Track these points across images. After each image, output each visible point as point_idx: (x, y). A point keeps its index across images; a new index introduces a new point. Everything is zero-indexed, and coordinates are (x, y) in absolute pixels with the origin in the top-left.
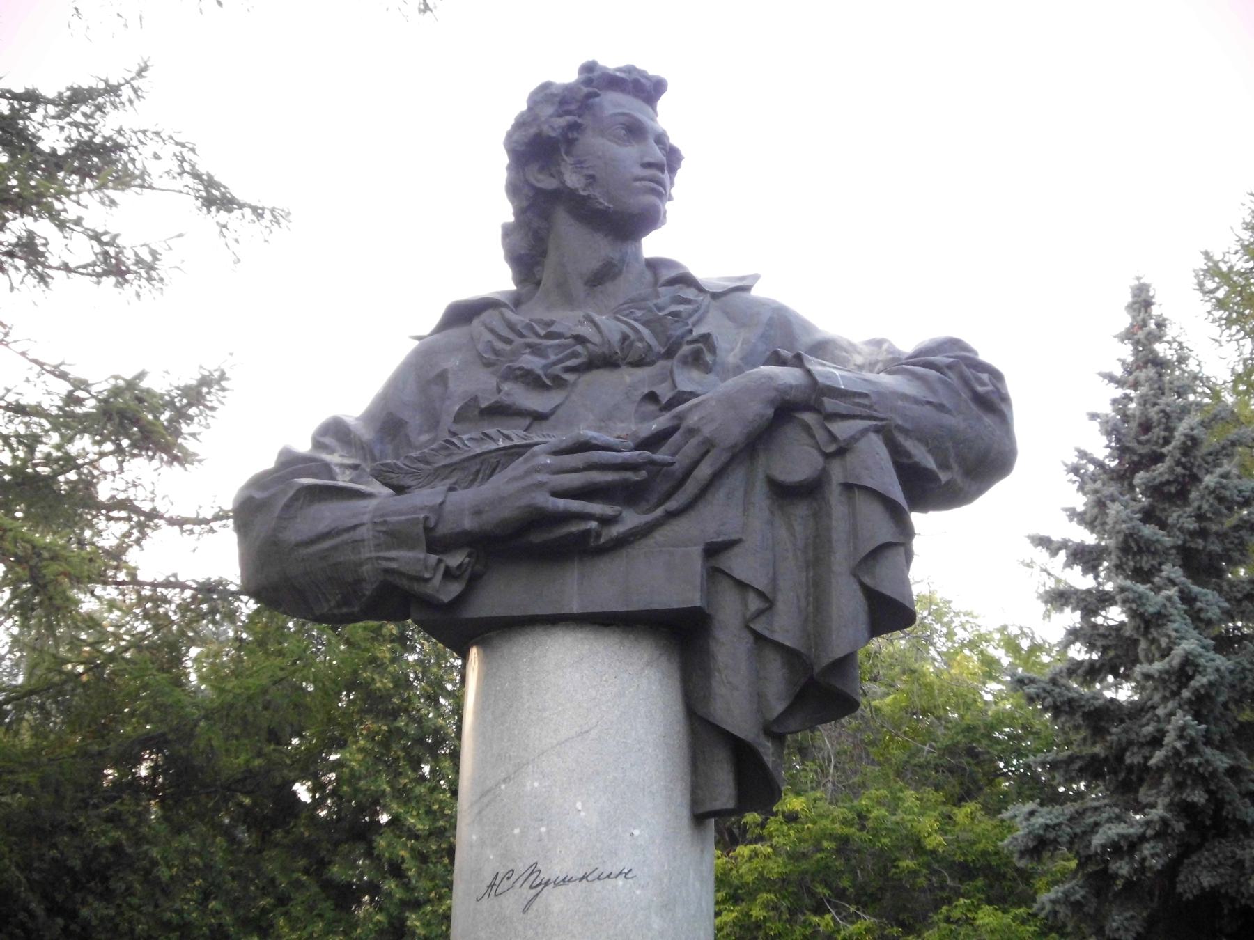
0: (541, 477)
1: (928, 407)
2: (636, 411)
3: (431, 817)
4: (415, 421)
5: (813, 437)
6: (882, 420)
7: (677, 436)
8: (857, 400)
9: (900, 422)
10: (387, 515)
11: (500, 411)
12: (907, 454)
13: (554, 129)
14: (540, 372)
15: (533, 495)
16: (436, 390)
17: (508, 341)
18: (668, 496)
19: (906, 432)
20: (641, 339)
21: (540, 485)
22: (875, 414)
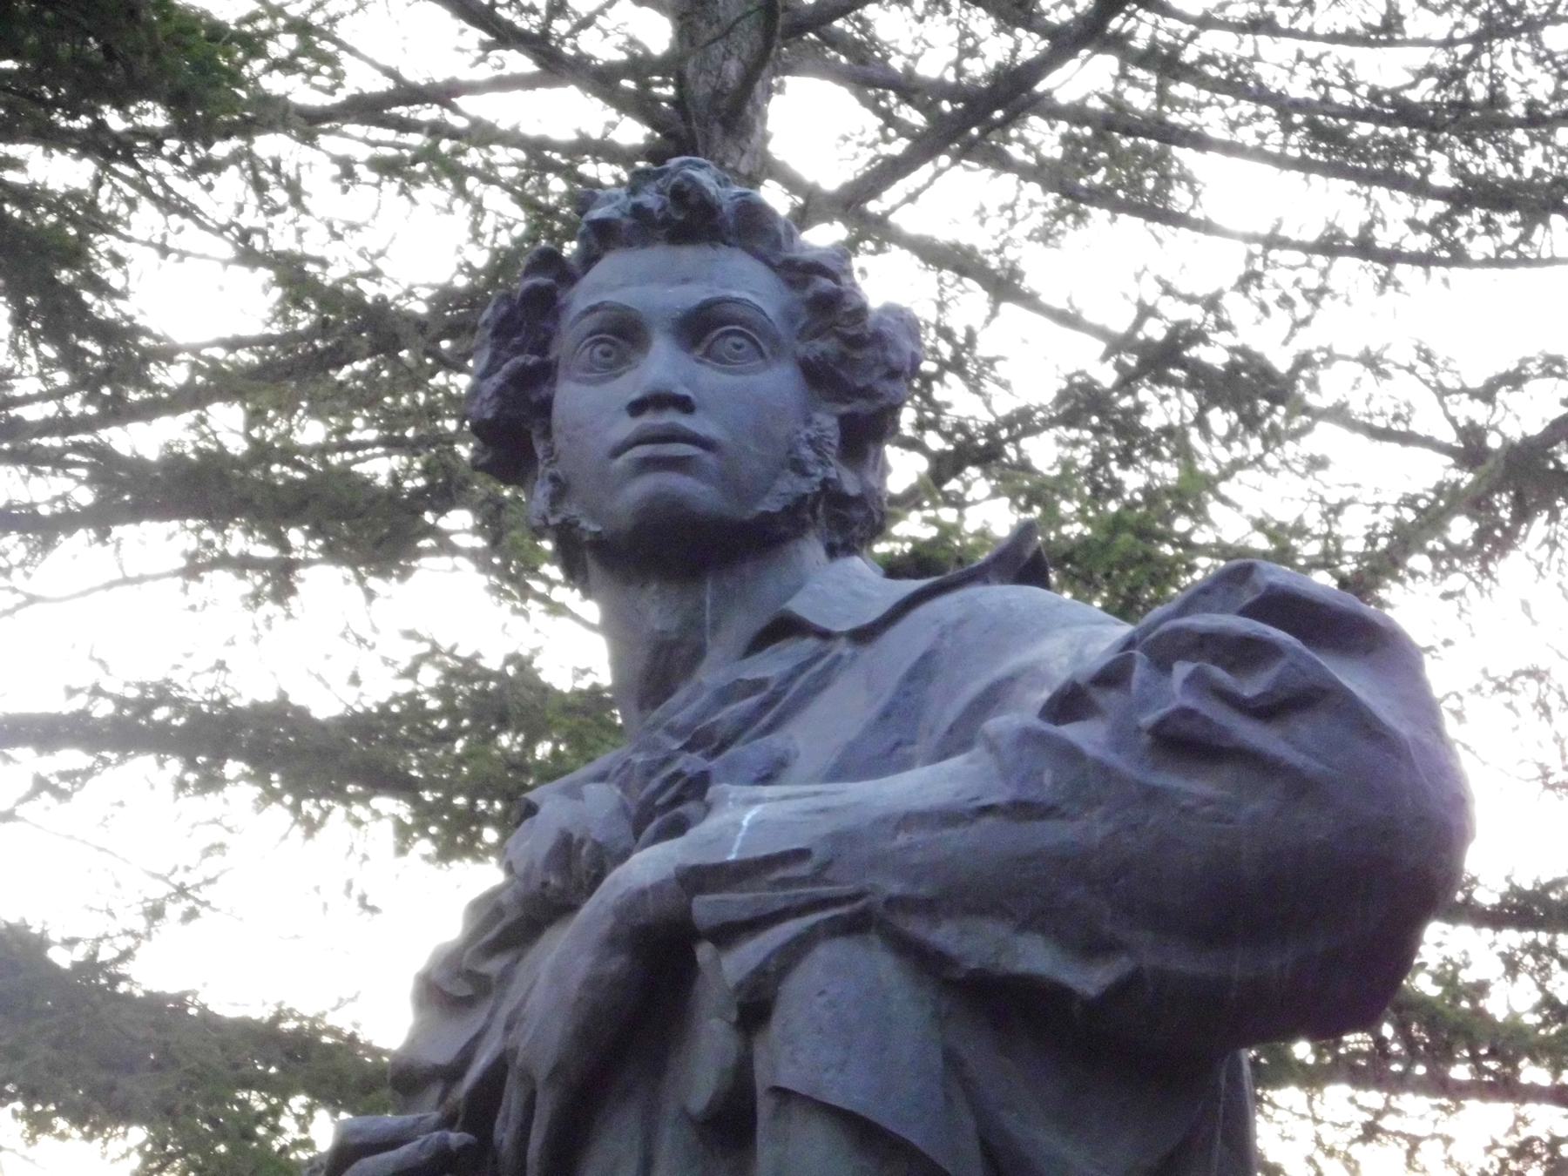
1: (988, 821)
8: (780, 873)
9: (895, 888)
19: (928, 908)
22: (824, 890)
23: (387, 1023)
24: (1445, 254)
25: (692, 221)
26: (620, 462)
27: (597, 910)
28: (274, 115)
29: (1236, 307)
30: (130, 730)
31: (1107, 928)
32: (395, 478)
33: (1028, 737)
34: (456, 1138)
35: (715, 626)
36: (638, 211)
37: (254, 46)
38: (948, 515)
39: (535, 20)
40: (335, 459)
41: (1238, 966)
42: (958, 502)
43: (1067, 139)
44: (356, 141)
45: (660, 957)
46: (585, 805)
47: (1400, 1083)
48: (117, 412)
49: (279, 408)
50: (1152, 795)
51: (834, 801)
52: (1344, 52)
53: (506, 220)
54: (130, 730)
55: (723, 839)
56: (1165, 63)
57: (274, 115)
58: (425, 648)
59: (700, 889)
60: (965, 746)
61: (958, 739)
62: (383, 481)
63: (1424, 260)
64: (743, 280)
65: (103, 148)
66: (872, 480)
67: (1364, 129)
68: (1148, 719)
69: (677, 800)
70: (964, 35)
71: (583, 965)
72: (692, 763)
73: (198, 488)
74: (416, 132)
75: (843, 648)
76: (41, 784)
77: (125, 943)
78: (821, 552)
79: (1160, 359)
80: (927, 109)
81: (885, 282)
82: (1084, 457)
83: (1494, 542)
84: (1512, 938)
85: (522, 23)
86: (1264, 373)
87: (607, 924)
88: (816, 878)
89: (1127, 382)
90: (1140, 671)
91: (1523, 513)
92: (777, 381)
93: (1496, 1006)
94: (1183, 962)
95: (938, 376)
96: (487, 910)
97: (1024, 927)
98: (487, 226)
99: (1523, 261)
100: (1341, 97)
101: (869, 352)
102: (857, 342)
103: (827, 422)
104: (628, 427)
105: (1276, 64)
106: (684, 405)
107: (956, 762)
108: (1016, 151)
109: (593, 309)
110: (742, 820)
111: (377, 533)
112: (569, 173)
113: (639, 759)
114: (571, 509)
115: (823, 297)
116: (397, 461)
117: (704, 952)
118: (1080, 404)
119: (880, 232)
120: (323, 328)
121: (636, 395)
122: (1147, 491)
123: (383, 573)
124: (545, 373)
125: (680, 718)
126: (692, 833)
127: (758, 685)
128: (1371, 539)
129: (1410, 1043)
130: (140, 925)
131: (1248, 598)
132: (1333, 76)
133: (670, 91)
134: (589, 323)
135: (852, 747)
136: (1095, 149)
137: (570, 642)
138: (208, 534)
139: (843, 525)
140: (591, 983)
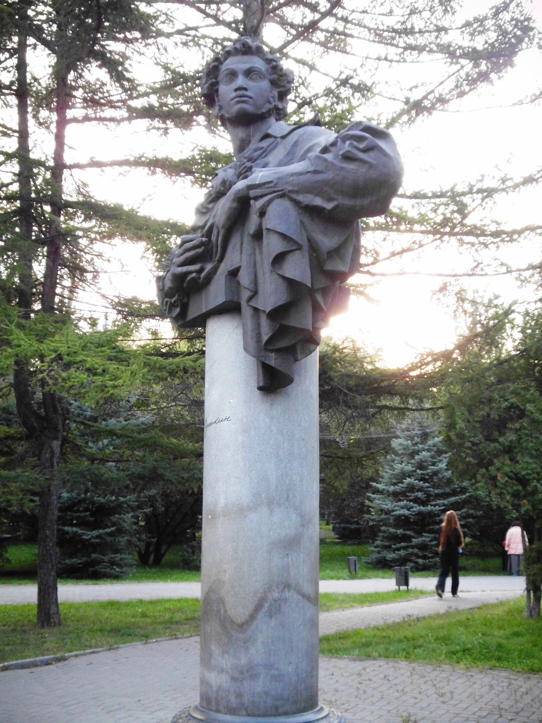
1: (309, 174)
3: (302, 319)
6: (282, 190)
8: (267, 186)
9: (290, 188)
19: (297, 192)
22: (276, 189)
23: (189, 219)
24: (402, 60)
25: (246, 50)
26: (233, 102)
27: (230, 194)
28: (160, 33)
29: (359, 71)
30: (138, 163)
31: (333, 195)
32: (188, 110)
33: (317, 157)
34: (204, 239)
35: (253, 136)
36: (236, 49)
37: (156, 18)
38: (301, 116)
39: (215, 12)
40: (176, 106)
41: (358, 202)
42: (304, 113)
43: (325, 36)
44: (178, 38)
45: (243, 203)
46: (226, 172)
47: (392, 230)
48: (131, 97)
49: (164, 96)
50: (342, 168)
51: (278, 171)
52: (382, 17)
53: (210, 55)
54: (138, 163)
55: (255, 179)
56: (345, 20)
57: (160, 33)
58: (195, 145)
59: (251, 189)
60: (304, 159)
61: (303, 158)
62: (186, 110)
63: (399, 61)
64: (257, 63)
65: (126, 40)
66: (285, 105)
67: (386, 34)
68: (341, 153)
69: (246, 172)
70: (304, 14)
71: (228, 205)
72: (249, 164)
73: (148, 113)
74: (189, 36)
75: (279, 140)
76: (120, 174)
77: (139, 205)
78: (274, 120)
79: (344, 83)
80: (296, 30)
81: (286, 64)
82: (329, 103)
83: (411, 121)
84: (414, 201)
85: (211, 13)
86: (366, 85)
87: (232, 197)
88: (274, 187)
89: (338, 87)
90: (339, 143)
91: (417, 115)
92: (265, 84)
93: (410, 215)
94: (348, 202)
95: (299, 86)
96: (209, 194)
97: (316, 196)
98: (205, 56)
99: (417, 62)
100: (381, 27)
101: (284, 77)
102: (281, 76)
103: (275, 93)
104: (234, 94)
105: (367, 20)
106: (246, 89)
107: (302, 163)
108: (314, 39)
109: (226, 70)
110: (259, 175)
111: (183, 120)
112: (221, 44)
113: (238, 163)
114: (223, 112)
115: (275, 69)
116: (188, 106)
117: (252, 202)
118: (329, 92)
119: (287, 56)
120: (173, 78)
121: (236, 87)
122: (342, 111)
123: (186, 129)
124: (217, 83)
125: (247, 155)
126: (249, 178)
127: (262, 148)
128: (387, 120)
129: (393, 222)
130: (141, 202)
131: (361, 128)
132: (380, 23)
133: (242, 26)
134: (226, 72)
135: (281, 160)
136: (331, 38)
137: (223, 142)
138: (151, 122)
139: (278, 114)
140: (230, 208)
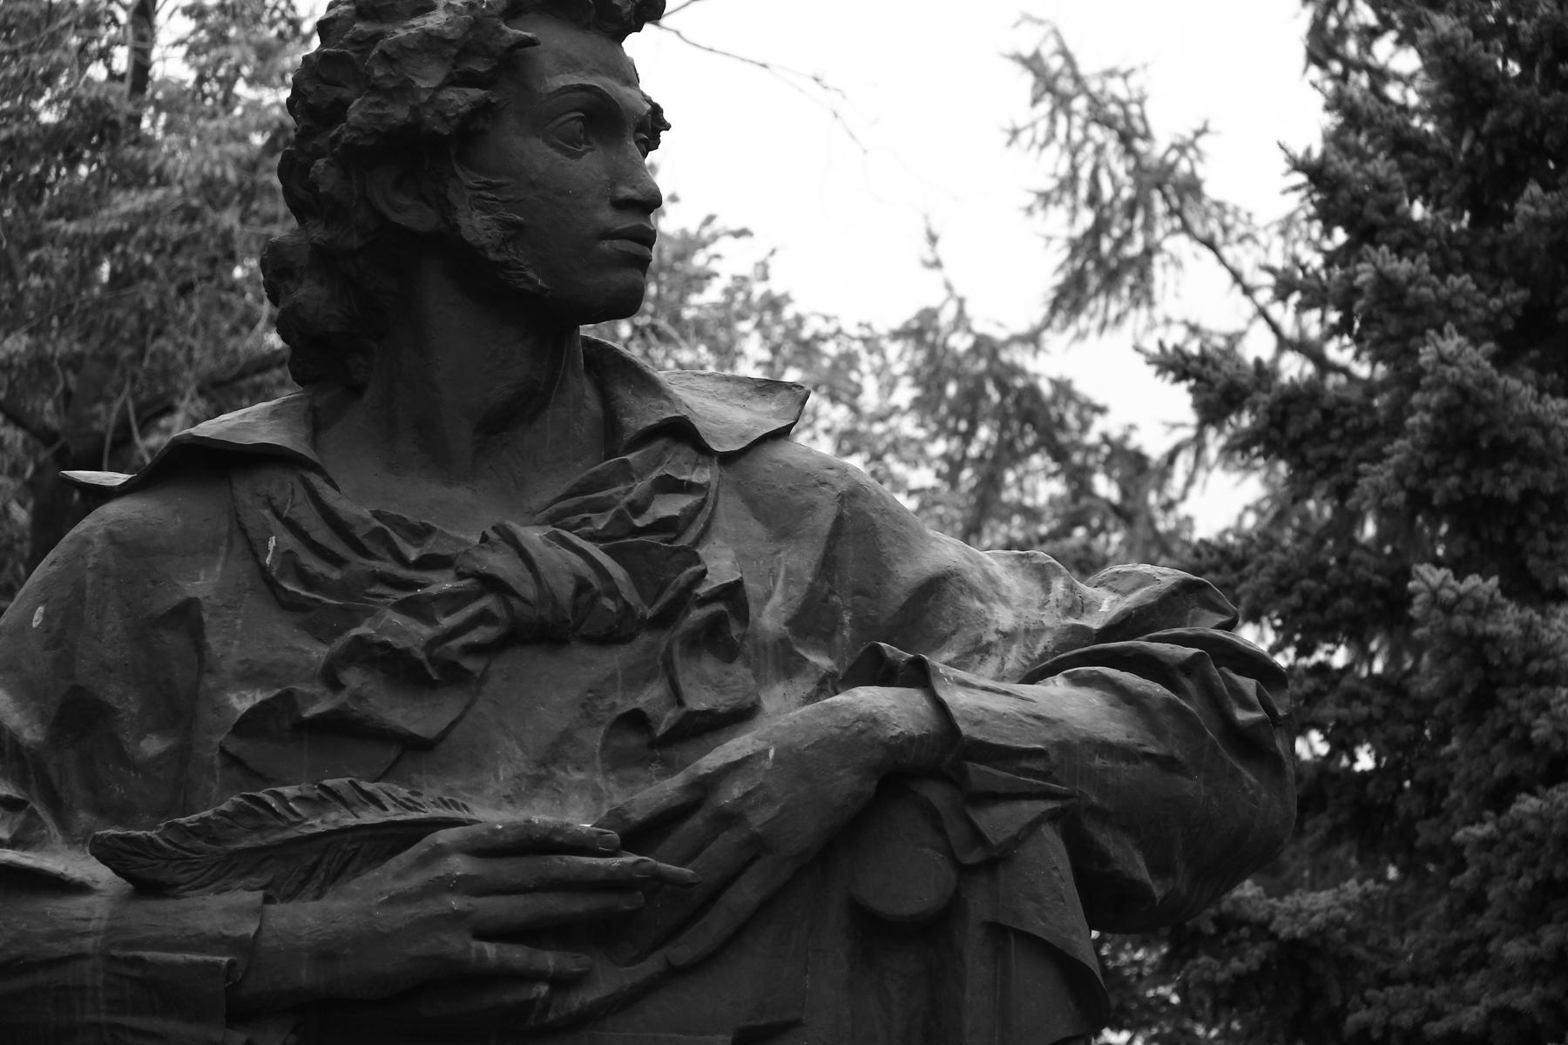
0: (456, 903)
1: (1147, 764)
2: (604, 747)
4: (125, 700)
5: (940, 830)
6: (1065, 797)
7: (696, 821)
8: (1025, 764)
10: (140, 945)
11: (345, 731)
12: (1103, 857)
13: (445, 120)
14: (422, 656)
15: (445, 937)
16: (173, 641)
17: (337, 561)
18: (672, 934)
20: (614, 593)
21: (457, 918)
